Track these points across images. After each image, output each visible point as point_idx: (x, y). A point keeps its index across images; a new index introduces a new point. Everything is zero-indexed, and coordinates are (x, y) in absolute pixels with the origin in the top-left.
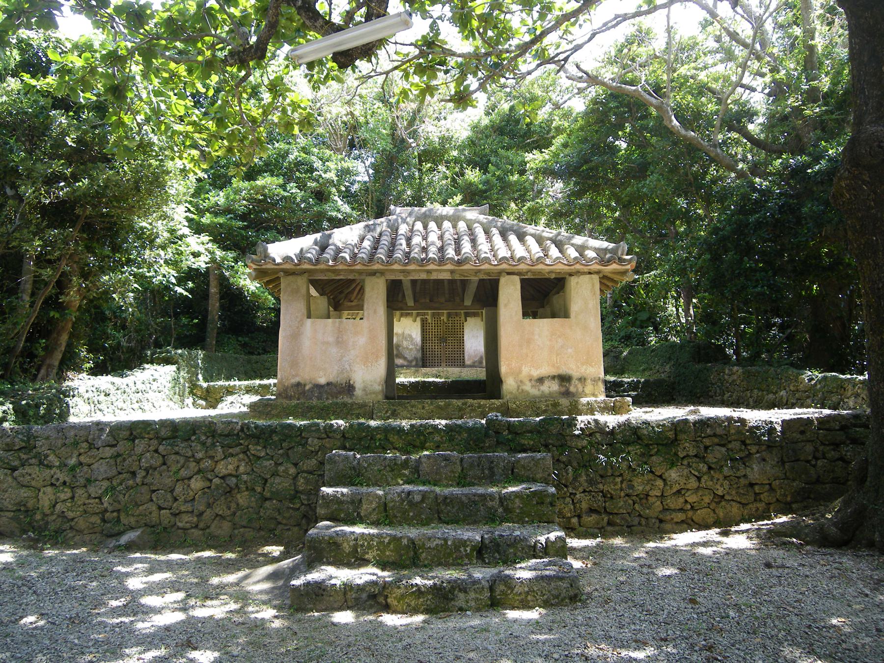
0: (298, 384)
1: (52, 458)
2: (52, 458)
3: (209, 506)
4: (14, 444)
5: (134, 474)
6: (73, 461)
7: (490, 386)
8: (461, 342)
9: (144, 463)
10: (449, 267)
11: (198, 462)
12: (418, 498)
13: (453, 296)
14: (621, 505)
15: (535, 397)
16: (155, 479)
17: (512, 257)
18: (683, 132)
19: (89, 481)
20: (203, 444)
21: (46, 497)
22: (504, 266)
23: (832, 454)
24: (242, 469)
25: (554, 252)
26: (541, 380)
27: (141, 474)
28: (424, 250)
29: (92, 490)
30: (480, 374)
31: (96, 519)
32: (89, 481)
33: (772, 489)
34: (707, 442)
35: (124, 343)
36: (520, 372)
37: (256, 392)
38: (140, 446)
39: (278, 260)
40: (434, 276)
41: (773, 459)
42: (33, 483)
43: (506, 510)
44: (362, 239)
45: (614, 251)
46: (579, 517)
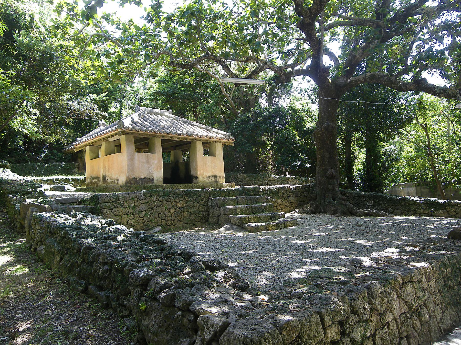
0: (134, 178)
1: (125, 204)
2: (125, 204)
3: (176, 217)
4: (111, 200)
5: (152, 209)
9: (156, 205)
20: (173, 197)
23: (303, 195)
24: (184, 205)
26: (209, 177)
29: (141, 215)
31: (142, 225)
32: (139, 212)
36: (203, 174)
42: (120, 214)
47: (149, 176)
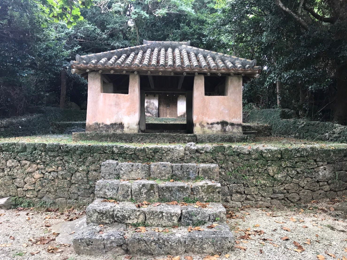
46: (231, 196)
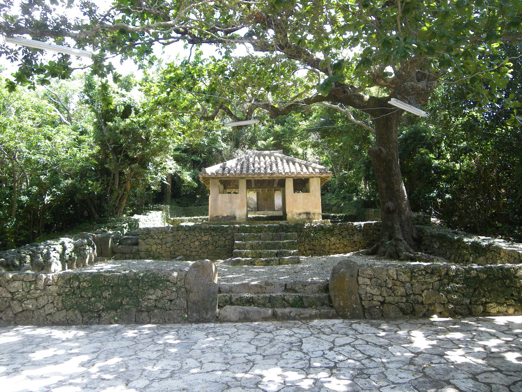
0: (217, 216)
1: (155, 236)
2: (155, 236)
3: (201, 249)
5: (178, 241)
6: (161, 237)
7: (284, 217)
8: (273, 201)
9: (181, 238)
10: (268, 176)
11: (197, 237)
12: (261, 243)
13: (268, 185)
14: (318, 248)
15: (297, 221)
16: (185, 242)
17: (290, 172)
18: (355, 121)
19: (166, 243)
21: (154, 247)
22: (287, 175)
25: (305, 170)
26: (300, 214)
27: (181, 241)
28: (259, 169)
29: (167, 245)
30: (280, 213)
31: (169, 253)
32: (166, 243)
33: (360, 243)
34: (342, 230)
35: (136, 203)
36: (293, 211)
37: (193, 222)
38: (180, 233)
39: (210, 174)
40: (263, 178)
41: (361, 234)
43: (284, 246)
44: (237, 165)
45: (324, 170)
47: (232, 214)
